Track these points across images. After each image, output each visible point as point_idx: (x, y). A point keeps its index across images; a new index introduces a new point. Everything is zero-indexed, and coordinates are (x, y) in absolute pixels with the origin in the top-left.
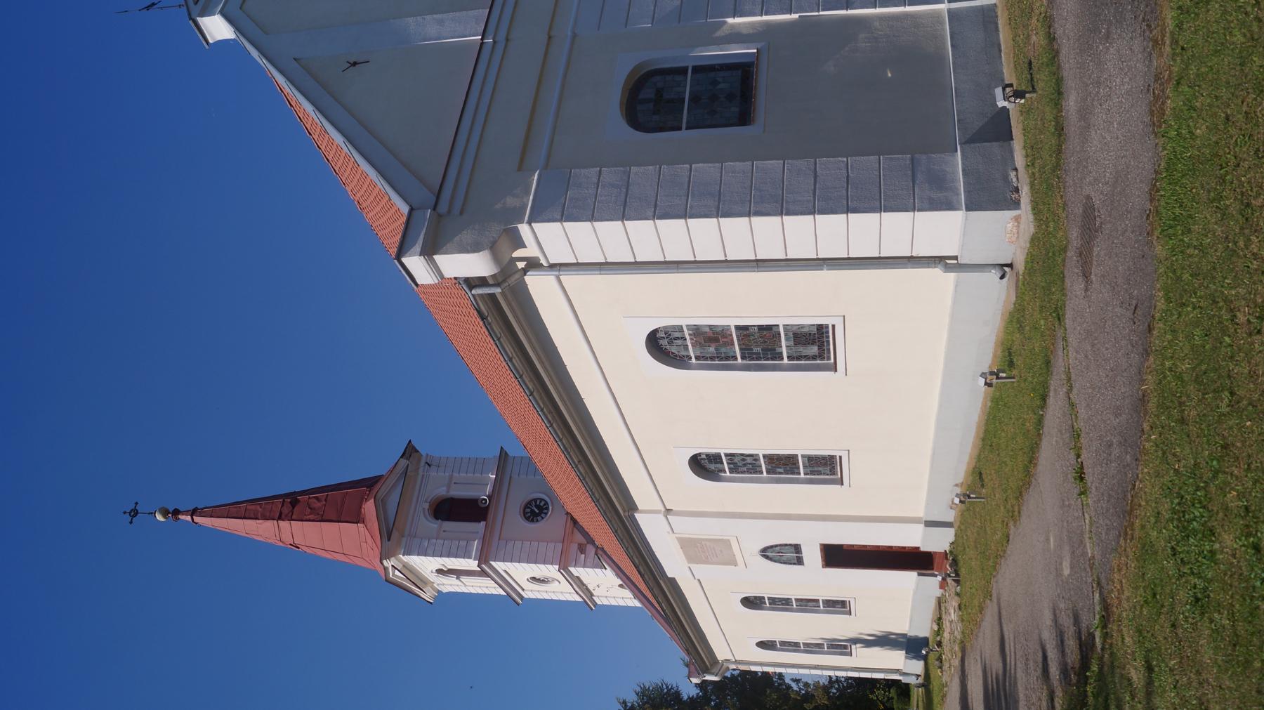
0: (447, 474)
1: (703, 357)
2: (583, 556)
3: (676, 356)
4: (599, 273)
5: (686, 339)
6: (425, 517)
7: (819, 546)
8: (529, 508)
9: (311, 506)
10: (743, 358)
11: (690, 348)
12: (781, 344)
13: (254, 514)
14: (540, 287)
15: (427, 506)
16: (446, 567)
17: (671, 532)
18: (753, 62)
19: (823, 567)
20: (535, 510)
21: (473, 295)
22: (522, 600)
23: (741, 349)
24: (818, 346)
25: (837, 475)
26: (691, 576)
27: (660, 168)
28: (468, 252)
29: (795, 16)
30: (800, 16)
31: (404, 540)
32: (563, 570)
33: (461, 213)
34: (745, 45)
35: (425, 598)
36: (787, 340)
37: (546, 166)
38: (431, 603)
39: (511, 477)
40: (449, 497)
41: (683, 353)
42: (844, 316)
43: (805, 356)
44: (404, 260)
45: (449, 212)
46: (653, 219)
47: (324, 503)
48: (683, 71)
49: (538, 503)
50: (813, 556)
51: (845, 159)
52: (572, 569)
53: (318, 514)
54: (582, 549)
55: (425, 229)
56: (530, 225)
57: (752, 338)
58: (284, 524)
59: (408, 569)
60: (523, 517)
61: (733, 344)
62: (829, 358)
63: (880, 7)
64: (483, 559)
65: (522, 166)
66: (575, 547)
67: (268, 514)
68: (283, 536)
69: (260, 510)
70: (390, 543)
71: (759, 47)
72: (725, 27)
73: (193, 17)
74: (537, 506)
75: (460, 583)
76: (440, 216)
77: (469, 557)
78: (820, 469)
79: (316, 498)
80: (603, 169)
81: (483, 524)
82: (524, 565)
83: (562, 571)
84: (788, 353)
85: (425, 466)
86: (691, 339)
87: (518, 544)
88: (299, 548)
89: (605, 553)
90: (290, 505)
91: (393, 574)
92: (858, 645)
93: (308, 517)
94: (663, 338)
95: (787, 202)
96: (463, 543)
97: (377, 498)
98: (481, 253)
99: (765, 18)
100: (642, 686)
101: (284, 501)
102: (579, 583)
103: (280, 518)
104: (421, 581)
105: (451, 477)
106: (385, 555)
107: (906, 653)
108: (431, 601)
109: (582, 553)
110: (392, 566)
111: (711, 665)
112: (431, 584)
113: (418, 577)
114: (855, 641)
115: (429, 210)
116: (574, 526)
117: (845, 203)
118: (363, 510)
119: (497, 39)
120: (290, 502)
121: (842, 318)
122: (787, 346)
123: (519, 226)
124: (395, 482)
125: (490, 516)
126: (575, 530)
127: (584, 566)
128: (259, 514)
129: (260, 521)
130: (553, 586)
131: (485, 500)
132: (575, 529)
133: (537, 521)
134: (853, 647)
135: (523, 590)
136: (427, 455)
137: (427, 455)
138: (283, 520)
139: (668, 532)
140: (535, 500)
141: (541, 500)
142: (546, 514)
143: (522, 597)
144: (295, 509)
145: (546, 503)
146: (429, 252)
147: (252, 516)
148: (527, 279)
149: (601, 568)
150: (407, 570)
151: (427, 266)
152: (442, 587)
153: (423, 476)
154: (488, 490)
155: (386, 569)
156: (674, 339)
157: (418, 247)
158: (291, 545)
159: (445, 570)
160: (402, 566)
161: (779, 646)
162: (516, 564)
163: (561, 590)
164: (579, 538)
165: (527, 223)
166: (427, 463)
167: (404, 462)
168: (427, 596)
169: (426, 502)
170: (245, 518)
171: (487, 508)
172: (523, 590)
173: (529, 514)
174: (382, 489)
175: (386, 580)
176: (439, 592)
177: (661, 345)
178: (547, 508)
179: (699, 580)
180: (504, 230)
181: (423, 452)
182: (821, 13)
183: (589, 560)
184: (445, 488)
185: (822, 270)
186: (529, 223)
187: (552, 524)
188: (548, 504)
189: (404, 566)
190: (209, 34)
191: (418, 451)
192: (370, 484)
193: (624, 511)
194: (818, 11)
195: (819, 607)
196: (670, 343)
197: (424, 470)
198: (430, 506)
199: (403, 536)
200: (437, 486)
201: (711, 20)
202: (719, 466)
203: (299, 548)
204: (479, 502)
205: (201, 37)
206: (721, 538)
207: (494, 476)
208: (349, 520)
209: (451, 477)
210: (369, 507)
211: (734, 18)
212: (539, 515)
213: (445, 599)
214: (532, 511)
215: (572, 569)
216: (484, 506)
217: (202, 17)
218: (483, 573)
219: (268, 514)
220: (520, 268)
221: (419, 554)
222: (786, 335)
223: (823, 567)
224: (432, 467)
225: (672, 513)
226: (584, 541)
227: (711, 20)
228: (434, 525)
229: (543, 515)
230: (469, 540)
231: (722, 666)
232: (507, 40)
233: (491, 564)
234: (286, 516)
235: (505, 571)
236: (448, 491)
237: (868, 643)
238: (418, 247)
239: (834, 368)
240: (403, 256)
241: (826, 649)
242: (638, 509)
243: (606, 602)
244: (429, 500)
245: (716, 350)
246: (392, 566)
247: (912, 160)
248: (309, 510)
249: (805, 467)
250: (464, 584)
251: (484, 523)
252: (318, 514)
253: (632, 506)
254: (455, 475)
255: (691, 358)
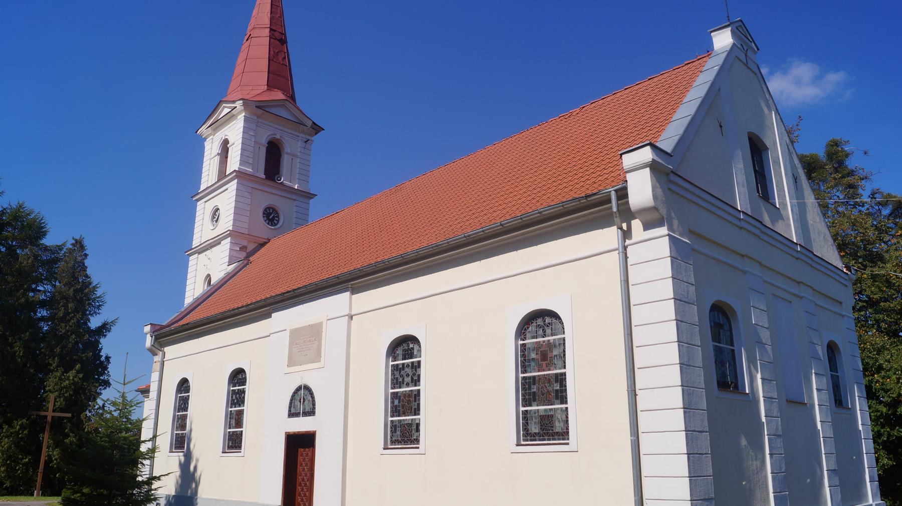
0: (299, 154)
1: (525, 349)
2: (238, 249)
3: (525, 330)
4: (622, 279)
5: (543, 337)
6: (271, 135)
7: (314, 430)
8: (273, 211)
9: (279, 53)
10: (524, 378)
11: (535, 340)
12: (540, 405)
13: (274, 12)
14: (609, 236)
15: (278, 137)
16: (230, 146)
17: (328, 318)
18: (738, 390)
19: (286, 433)
20: (271, 216)
21: (610, 191)
22: (196, 200)
23: (534, 377)
24: (539, 433)
25: (391, 445)
26: (273, 331)
27: (697, 325)
28: (653, 191)
29: (764, 419)
30: (764, 422)
31: (256, 118)
32: (229, 233)
33: (669, 189)
34: (750, 386)
35: (203, 127)
36: (545, 410)
37: (694, 250)
38: (197, 132)
39: (295, 200)
40: (282, 153)
41: (528, 335)
42: (577, 452)
43: (527, 423)
44: (648, 148)
45: (670, 181)
46: (676, 320)
47: (281, 63)
48: (732, 345)
49: (276, 218)
50: (301, 425)
51: (710, 452)
52: (229, 240)
53: (273, 58)
54: (243, 248)
55: (664, 163)
56: (667, 235)
57: (547, 385)
58: (267, 32)
59: (230, 118)
60: (268, 206)
61: (539, 371)
62: (524, 440)
63: (772, 477)
64: (239, 174)
65: (692, 233)
66: (245, 243)
67: (274, 21)
68: (257, 30)
69: (277, 16)
70: (254, 107)
71: (750, 395)
72: (755, 372)
73: (732, 25)
74: (274, 217)
75: (213, 155)
76: (668, 175)
77: (240, 164)
78: (398, 433)
79: (285, 58)
80: (694, 286)
81: (264, 177)
82: (233, 204)
83: (229, 232)
84: (531, 411)
85: (306, 139)
86: (544, 341)
87: (249, 202)
88: (247, 40)
89: (245, 266)
90: (280, 38)
91: (225, 107)
92: (182, 459)
93: (271, 50)
94: (545, 321)
95: (689, 412)
96: (251, 161)
97: (286, 102)
98: (652, 200)
99: (762, 399)
100: (98, 286)
101: (283, 34)
102: (215, 243)
103: (271, 30)
104: (218, 125)
105: (297, 156)
106: (246, 103)
107: (174, 496)
108: (198, 133)
109: (240, 248)
110: (236, 107)
111: (159, 342)
112: (213, 133)
113: (222, 124)
114: (188, 456)
115: (672, 168)
116: (259, 244)
117: (692, 452)
118: (276, 90)
119: (742, 221)
120: (282, 38)
121: (576, 450)
122: (538, 410)
123: (666, 228)
124: (297, 117)
125: (269, 183)
126: (256, 245)
127: (231, 249)
128: (274, 15)
129: (269, 15)
130: (208, 224)
131: (280, 180)
132: (257, 244)
133: (264, 217)
134: (182, 454)
135: (205, 202)
136: (313, 141)
137: (313, 141)
138: (270, 32)
139: (327, 316)
140: (278, 217)
141: (278, 221)
142: (268, 224)
143: (198, 200)
144: (278, 42)
145: (276, 225)
146: (653, 167)
147: (273, 10)
148: (615, 228)
149: (229, 262)
150: (230, 117)
151: (642, 163)
152: (210, 141)
153: (299, 136)
154: (287, 183)
155: (234, 102)
156: (543, 330)
157: (656, 158)
158: (250, 35)
159: (228, 146)
160: (235, 114)
161: (179, 395)
162: (234, 198)
163: (203, 231)
164: (251, 247)
165: (669, 234)
166: (309, 140)
167: (309, 123)
168: (203, 130)
169: (281, 136)
170: (272, 4)
171: (274, 180)
172: (205, 202)
173: (268, 211)
174: (290, 106)
175: (221, 101)
176: (205, 139)
177: (537, 320)
178: (272, 225)
179: (269, 336)
180: (663, 217)
181: (315, 138)
182: (766, 437)
183: (235, 253)
184: (289, 151)
185: (631, 436)
186: (669, 235)
187: (262, 228)
188: (275, 226)
189: (234, 115)
190: (716, 34)
191: (316, 134)
192: (293, 98)
193: (351, 284)
194: (768, 435)
195: (230, 428)
196: (539, 326)
197: (303, 137)
198: (278, 139)
199: (258, 117)
200: (291, 146)
201: (759, 363)
202: (401, 357)
203: (247, 40)
204: (278, 176)
205: (716, 28)
206: (323, 354)
207: (296, 188)
208: (269, 80)
209: (297, 156)
210: (279, 95)
211: (761, 378)
212: (268, 218)
213: (200, 143)
214: (270, 214)
215: (229, 240)
216: (276, 178)
217: (731, 31)
218: (222, 174)
219: (274, 21)
220: (623, 224)
221: (244, 127)
222: (551, 410)
223: (286, 433)
224: (305, 144)
225: (350, 320)
226: (248, 250)
227: (759, 363)
228: (264, 141)
229: (267, 221)
230: (252, 165)
231: (159, 350)
232: (741, 228)
233: (235, 179)
234: (273, 34)
235: (227, 189)
236: (287, 153)
237: (185, 467)
238: (656, 158)
239: (518, 445)
240: (651, 148)
241: (175, 432)
242: (353, 295)
243: (191, 263)
244: (282, 139)
245: (533, 359)
246: (236, 107)
247: (712, 499)
248: (276, 52)
249: (400, 421)
250: (212, 158)
251: (265, 178)
252: (273, 58)
253: (355, 291)
254: (298, 160)
255: (523, 340)
